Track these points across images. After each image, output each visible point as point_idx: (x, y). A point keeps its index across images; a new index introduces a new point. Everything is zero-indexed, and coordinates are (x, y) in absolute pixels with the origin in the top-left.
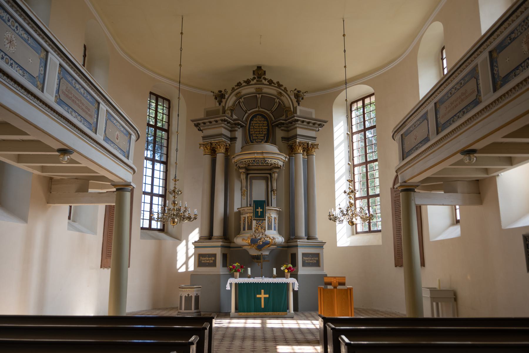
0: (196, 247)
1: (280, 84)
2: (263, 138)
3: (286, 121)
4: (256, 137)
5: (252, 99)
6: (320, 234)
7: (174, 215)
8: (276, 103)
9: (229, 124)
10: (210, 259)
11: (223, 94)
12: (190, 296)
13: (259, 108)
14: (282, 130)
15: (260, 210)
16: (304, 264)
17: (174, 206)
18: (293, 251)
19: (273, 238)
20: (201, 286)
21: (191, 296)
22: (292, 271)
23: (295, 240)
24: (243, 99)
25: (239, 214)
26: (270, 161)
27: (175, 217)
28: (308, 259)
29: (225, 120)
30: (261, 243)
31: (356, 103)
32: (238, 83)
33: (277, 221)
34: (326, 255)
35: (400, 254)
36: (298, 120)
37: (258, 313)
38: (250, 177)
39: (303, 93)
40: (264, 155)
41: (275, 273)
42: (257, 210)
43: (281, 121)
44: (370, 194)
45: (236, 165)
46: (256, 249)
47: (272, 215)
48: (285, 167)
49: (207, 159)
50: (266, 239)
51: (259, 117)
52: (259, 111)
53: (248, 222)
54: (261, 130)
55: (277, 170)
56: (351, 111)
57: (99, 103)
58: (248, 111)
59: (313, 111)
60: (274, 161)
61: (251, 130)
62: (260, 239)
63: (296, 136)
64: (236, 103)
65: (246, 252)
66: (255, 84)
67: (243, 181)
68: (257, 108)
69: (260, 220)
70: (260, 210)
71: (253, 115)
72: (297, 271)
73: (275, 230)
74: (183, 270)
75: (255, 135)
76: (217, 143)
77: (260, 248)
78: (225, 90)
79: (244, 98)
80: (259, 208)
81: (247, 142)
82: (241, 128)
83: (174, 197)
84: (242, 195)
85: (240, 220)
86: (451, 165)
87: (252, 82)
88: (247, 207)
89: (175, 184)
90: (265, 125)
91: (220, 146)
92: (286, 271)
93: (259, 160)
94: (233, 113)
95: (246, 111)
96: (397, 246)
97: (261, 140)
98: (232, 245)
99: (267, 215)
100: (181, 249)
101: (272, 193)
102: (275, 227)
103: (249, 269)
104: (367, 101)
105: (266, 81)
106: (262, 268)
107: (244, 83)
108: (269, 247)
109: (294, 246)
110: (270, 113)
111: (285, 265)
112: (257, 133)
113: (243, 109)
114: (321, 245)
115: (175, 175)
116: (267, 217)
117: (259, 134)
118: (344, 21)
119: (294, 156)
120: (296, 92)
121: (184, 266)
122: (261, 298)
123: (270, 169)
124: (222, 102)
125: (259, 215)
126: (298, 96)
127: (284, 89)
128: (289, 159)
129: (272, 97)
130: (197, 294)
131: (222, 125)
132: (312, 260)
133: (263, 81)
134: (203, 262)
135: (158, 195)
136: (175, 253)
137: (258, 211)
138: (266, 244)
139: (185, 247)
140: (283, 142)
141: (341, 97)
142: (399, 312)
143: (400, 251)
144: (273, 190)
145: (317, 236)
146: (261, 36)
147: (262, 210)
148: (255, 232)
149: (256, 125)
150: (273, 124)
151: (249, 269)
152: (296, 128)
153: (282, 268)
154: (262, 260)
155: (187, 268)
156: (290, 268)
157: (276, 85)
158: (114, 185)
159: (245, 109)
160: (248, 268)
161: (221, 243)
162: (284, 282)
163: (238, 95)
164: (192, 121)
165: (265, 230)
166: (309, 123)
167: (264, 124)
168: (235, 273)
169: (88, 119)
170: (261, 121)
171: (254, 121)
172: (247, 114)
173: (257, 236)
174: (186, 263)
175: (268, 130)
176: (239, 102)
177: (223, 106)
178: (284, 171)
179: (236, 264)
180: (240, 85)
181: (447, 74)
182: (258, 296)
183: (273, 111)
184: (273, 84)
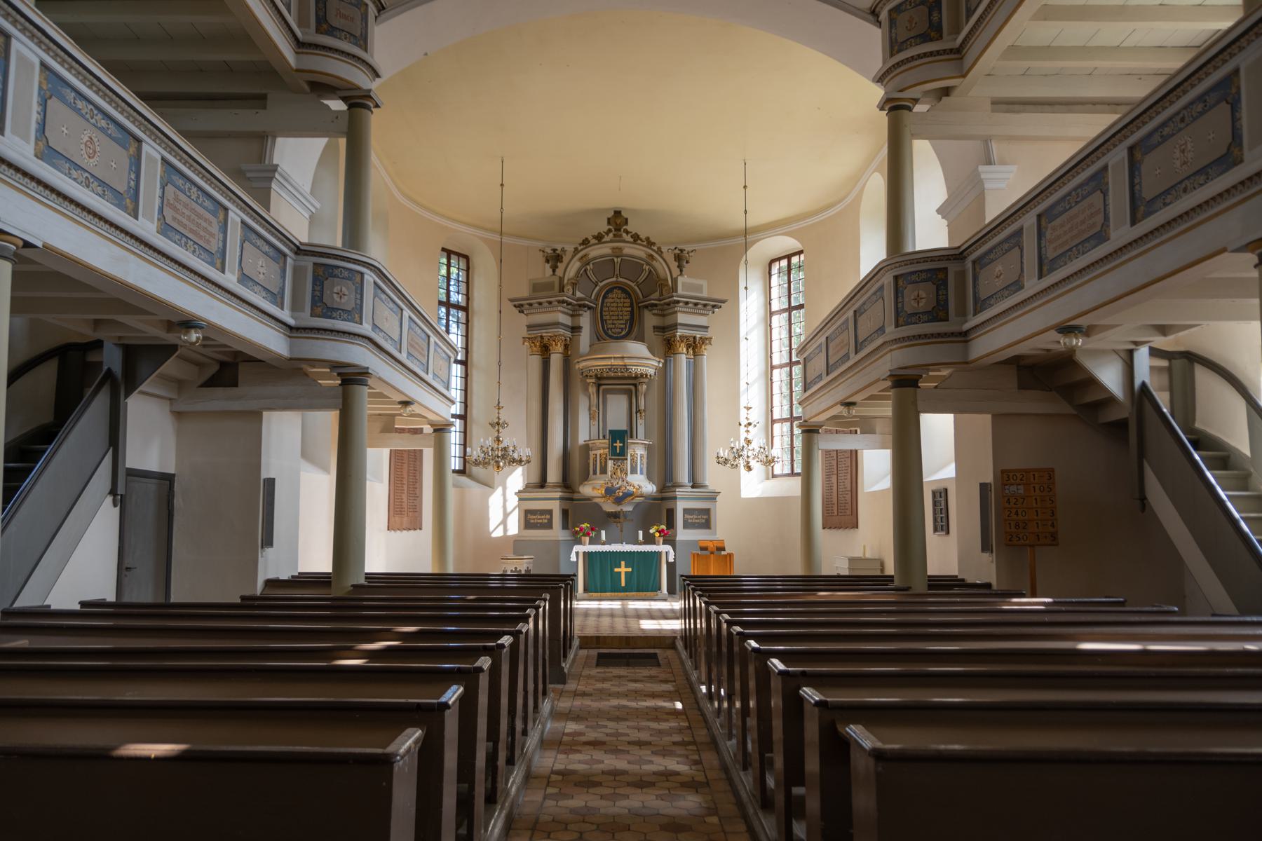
0: (520, 500)
2: (623, 326)
3: (660, 301)
4: (613, 324)
5: (606, 265)
6: (713, 476)
7: (498, 457)
9: (569, 307)
10: (543, 517)
11: (558, 255)
13: (617, 277)
14: (654, 314)
15: (618, 444)
17: (498, 444)
18: (669, 505)
20: (532, 557)
22: (666, 534)
23: (673, 489)
24: (591, 265)
25: (586, 448)
27: (500, 459)
29: (563, 302)
30: (621, 494)
31: (778, 262)
32: (583, 241)
33: (645, 461)
34: (721, 512)
36: (678, 302)
37: (616, 594)
38: (604, 390)
39: (688, 253)
40: (626, 361)
41: (641, 538)
42: (615, 444)
43: (653, 302)
45: (582, 373)
46: (613, 503)
47: (638, 451)
49: (536, 361)
50: (628, 487)
51: (618, 292)
52: (617, 282)
53: (601, 463)
54: (621, 313)
55: (646, 380)
56: (770, 275)
57: (429, 337)
58: (599, 284)
59: (704, 283)
61: (604, 313)
62: (619, 488)
63: (675, 326)
64: (581, 273)
65: (598, 506)
66: (611, 241)
67: (592, 396)
68: (613, 277)
69: (619, 459)
70: (618, 444)
71: (607, 289)
72: (676, 536)
73: (642, 473)
74: (498, 533)
75: (611, 322)
76: (551, 337)
77: (619, 501)
78: (563, 250)
79: (593, 264)
80: (618, 441)
81: (600, 338)
82: (589, 312)
83: (498, 431)
84: (590, 418)
86: (880, 391)
87: (606, 238)
88: (599, 439)
89: (499, 413)
90: (626, 305)
92: (657, 534)
93: (617, 369)
97: (620, 330)
98: (576, 496)
99: (630, 452)
100: (495, 501)
101: (638, 414)
102: (641, 469)
103: (603, 533)
104: (795, 260)
105: (629, 235)
106: (622, 531)
108: (632, 499)
111: (655, 527)
112: (614, 318)
113: (591, 280)
114: (713, 497)
116: (629, 455)
117: (618, 319)
119: (672, 355)
120: (677, 251)
121: (501, 527)
122: (620, 573)
123: (636, 378)
124: (557, 267)
125: (618, 452)
126: (680, 258)
128: (665, 364)
130: (528, 568)
131: (559, 308)
133: (624, 235)
134: (532, 521)
136: (485, 508)
137: (616, 447)
138: (628, 495)
139: (502, 498)
140: (656, 333)
141: (753, 252)
145: (707, 483)
146: (620, 177)
147: (621, 445)
150: (640, 305)
151: (603, 533)
152: (676, 312)
153: (652, 531)
154: (621, 520)
155: (505, 530)
156: (663, 530)
157: (645, 243)
158: (432, 425)
159: (594, 279)
161: (560, 494)
164: (511, 300)
165: (626, 474)
166: (696, 304)
168: (583, 538)
169: (419, 357)
170: (620, 298)
172: (598, 288)
173: (615, 483)
174: (504, 522)
175: (632, 313)
176: (585, 271)
177: (560, 277)
178: (656, 383)
179: (585, 525)
182: (616, 570)
184: (639, 242)
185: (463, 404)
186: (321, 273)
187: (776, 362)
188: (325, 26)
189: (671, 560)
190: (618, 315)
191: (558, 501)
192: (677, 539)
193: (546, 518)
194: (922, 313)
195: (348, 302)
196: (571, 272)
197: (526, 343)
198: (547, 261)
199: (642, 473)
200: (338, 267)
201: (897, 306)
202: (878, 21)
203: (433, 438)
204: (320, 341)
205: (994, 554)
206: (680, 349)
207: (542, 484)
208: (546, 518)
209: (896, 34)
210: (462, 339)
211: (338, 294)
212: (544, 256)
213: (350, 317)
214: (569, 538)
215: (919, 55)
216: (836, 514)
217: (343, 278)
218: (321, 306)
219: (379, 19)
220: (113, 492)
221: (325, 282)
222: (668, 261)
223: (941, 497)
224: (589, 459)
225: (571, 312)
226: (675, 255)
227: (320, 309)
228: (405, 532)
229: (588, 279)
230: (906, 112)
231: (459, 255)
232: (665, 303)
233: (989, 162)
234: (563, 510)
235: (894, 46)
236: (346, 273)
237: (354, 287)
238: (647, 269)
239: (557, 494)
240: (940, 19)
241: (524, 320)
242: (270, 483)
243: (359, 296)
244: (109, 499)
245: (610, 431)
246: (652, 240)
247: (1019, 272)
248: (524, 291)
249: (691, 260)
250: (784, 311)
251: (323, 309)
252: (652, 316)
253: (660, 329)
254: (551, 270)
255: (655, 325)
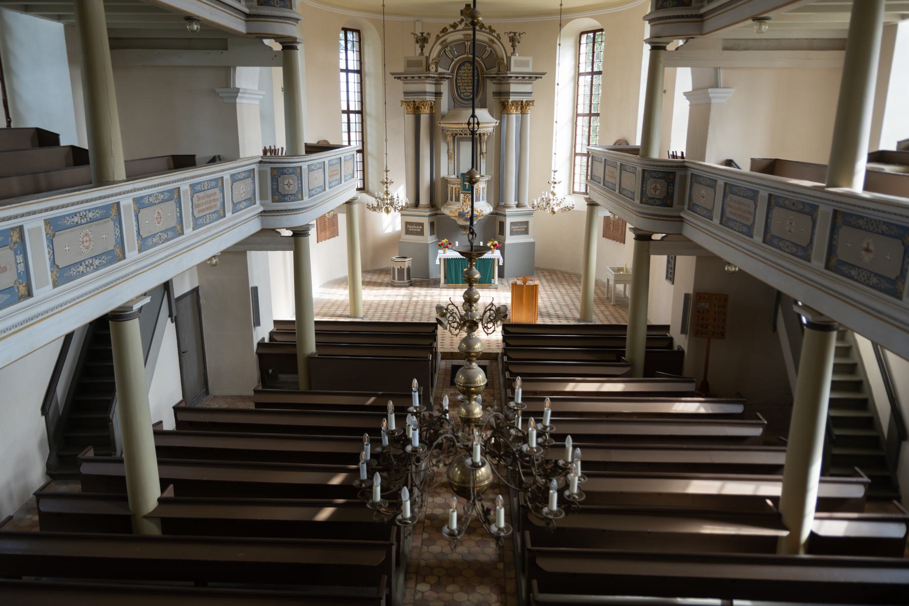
4: (464, 89)
7: (387, 204)
9: (434, 79)
10: (418, 227)
13: (467, 54)
14: (494, 83)
16: (512, 233)
18: (501, 219)
21: (404, 269)
24: (449, 48)
28: (515, 227)
33: (485, 191)
36: (511, 77)
44: (593, 112)
47: (481, 186)
49: (410, 118)
53: (456, 194)
56: (580, 44)
59: (530, 59)
63: (508, 93)
66: (463, 30)
68: (465, 54)
75: (463, 88)
87: (460, 27)
89: (387, 175)
102: (483, 197)
112: (465, 84)
113: (449, 57)
117: (468, 86)
124: (424, 47)
125: (467, 188)
134: (410, 230)
135: (355, 112)
140: (495, 97)
149: (464, 75)
150: (484, 76)
152: (509, 83)
156: (496, 245)
157: (488, 31)
163: (444, 43)
170: (470, 70)
172: (454, 62)
173: (465, 209)
176: (445, 51)
184: (484, 29)
185: (360, 103)
186: (276, 173)
187: (580, 111)
189: (501, 264)
190: (468, 83)
191: (427, 218)
193: (418, 229)
195: (293, 189)
196: (434, 54)
198: (417, 42)
199: (483, 200)
203: (345, 208)
204: (279, 217)
205: (688, 336)
207: (417, 204)
208: (418, 229)
210: (356, 53)
211: (287, 185)
212: (414, 38)
214: (435, 240)
215: (674, 16)
216: (612, 230)
217: (290, 174)
218: (279, 195)
220: (170, 315)
222: (506, 49)
224: (448, 188)
225: (434, 82)
226: (510, 37)
228: (327, 240)
230: (662, 51)
231: (353, 30)
232: (501, 77)
233: (716, 86)
234: (431, 223)
236: (291, 170)
237: (296, 177)
238: (489, 50)
242: (255, 289)
243: (300, 182)
244: (169, 319)
245: (462, 174)
246: (493, 28)
247: (712, 206)
248: (401, 68)
250: (588, 74)
252: (493, 84)
254: (420, 49)
255: (494, 91)
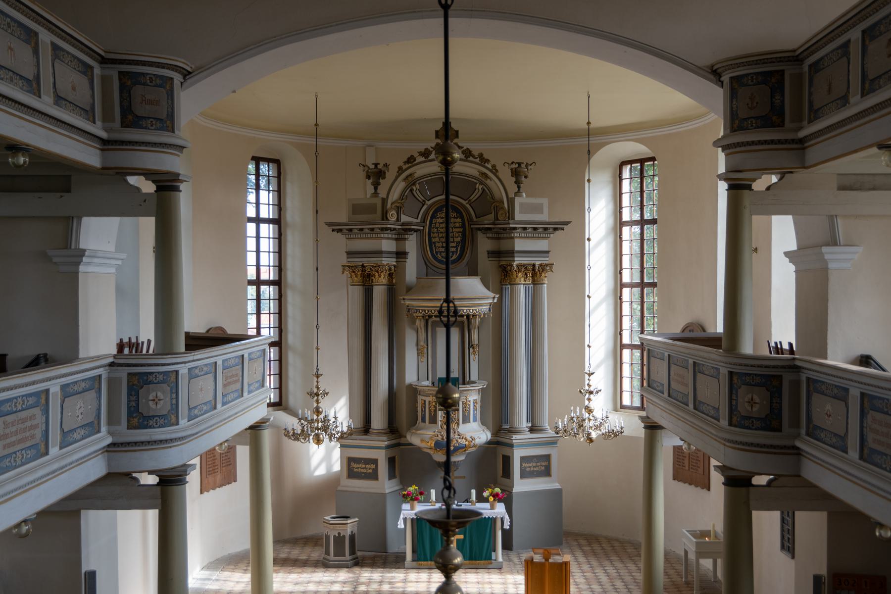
1: (484, 158)
8: (477, 191)
10: (367, 466)
12: (341, 535)
14: (488, 237)
16: (524, 475)
18: (505, 451)
19: (471, 439)
21: (344, 536)
24: (418, 186)
26: (467, 310)
28: (530, 465)
32: (409, 159)
35: (680, 462)
36: (515, 228)
48: (492, 313)
49: (357, 292)
50: (459, 440)
53: (430, 411)
56: (621, 179)
59: (545, 201)
60: (472, 310)
61: (433, 235)
63: (511, 253)
64: (406, 194)
67: (419, 329)
84: (418, 353)
85: (416, 401)
89: (318, 382)
90: (457, 225)
91: (378, 273)
94: (400, 212)
95: (423, 201)
96: (677, 455)
101: (471, 350)
102: (475, 416)
107: (419, 156)
109: (505, 443)
110: (466, 204)
115: (317, 366)
118: (589, 97)
120: (514, 166)
124: (379, 184)
126: (517, 174)
127: (491, 168)
129: (469, 180)
130: (352, 532)
132: (538, 466)
134: (356, 470)
140: (491, 259)
141: (598, 157)
142: (674, 552)
143: (681, 461)
144: (472, 345)
148: (442, 427)
150: (472, 226)
152: (513, 238)
157: (478, 160)
159: (421, 198)
160: (432, 490)
162: (487, 517)
163: (410, 179)
165: (458, 424)
167: (456, 223)
171: (438, 218)
172: (425, 207)
175: (464, 234)
176: (411, 191)
180: (413, 162)
181: (769, 170)
183: (474, 199)
186: (136, 382)
188: (130, 117)
189: (507, 526)
192: (513, 491)
194: (756, 419)
196: (395, 195)
197: (345, 272)
198: (368, 177)
200: (151, 373)
201: (731, 402)
202: (720, 81)
206: (518, 279)
207: (366, 428)
209: (737, 107)
213: (166, 421)
214: (397, 488)
215: (759, 141)
217: (158, 383)
219: (185, 85)
221: (140, 391)
223: (788, 515)
225: (396, 236)
227: (136, 420)
229: (415, 199)
232: (500, 228)
235: (735, 122)
236: (161, 377)
237: (169, 388)
239: (383, 443)
240: (783, 102)
241: (341, 243)
242: (91, 576)
243: (174, 396)
246: (486, 156)
249: (530, 174)
251: (139, 420)
253: (496, 254)
